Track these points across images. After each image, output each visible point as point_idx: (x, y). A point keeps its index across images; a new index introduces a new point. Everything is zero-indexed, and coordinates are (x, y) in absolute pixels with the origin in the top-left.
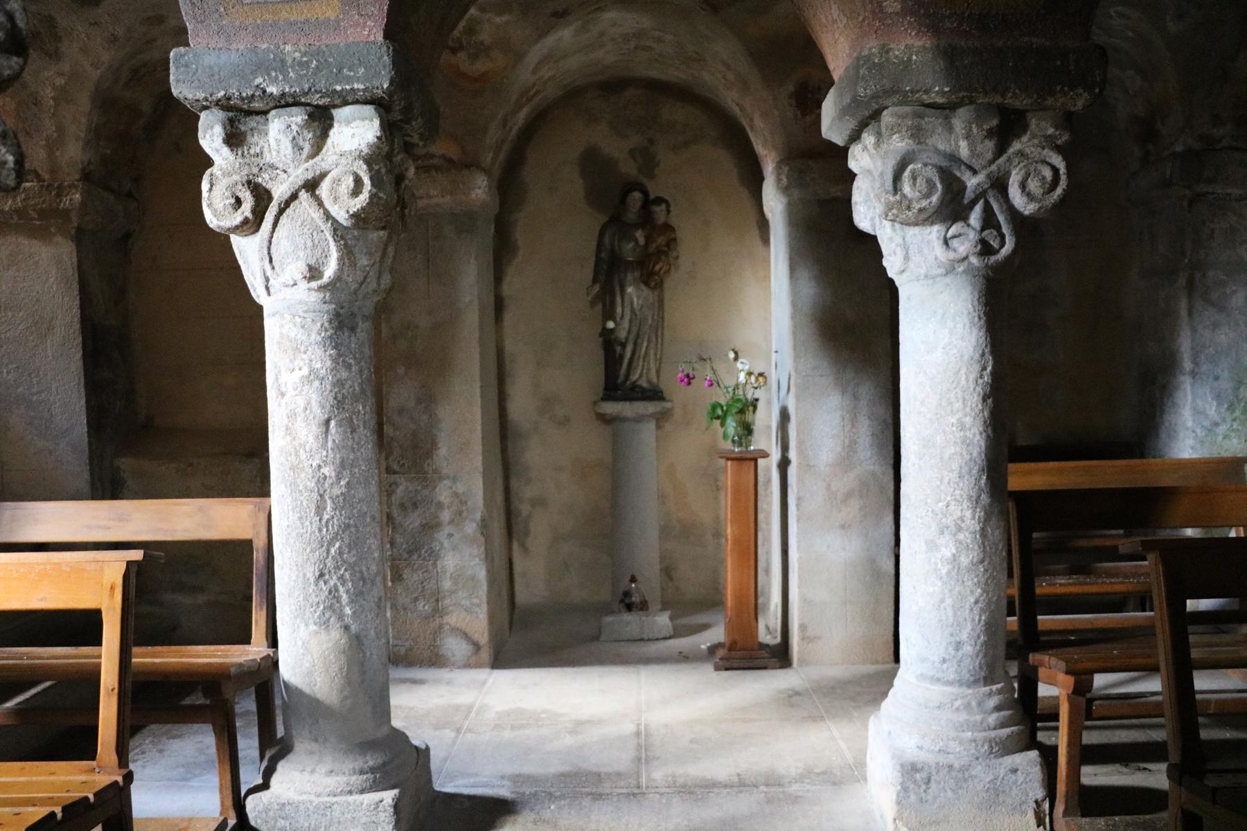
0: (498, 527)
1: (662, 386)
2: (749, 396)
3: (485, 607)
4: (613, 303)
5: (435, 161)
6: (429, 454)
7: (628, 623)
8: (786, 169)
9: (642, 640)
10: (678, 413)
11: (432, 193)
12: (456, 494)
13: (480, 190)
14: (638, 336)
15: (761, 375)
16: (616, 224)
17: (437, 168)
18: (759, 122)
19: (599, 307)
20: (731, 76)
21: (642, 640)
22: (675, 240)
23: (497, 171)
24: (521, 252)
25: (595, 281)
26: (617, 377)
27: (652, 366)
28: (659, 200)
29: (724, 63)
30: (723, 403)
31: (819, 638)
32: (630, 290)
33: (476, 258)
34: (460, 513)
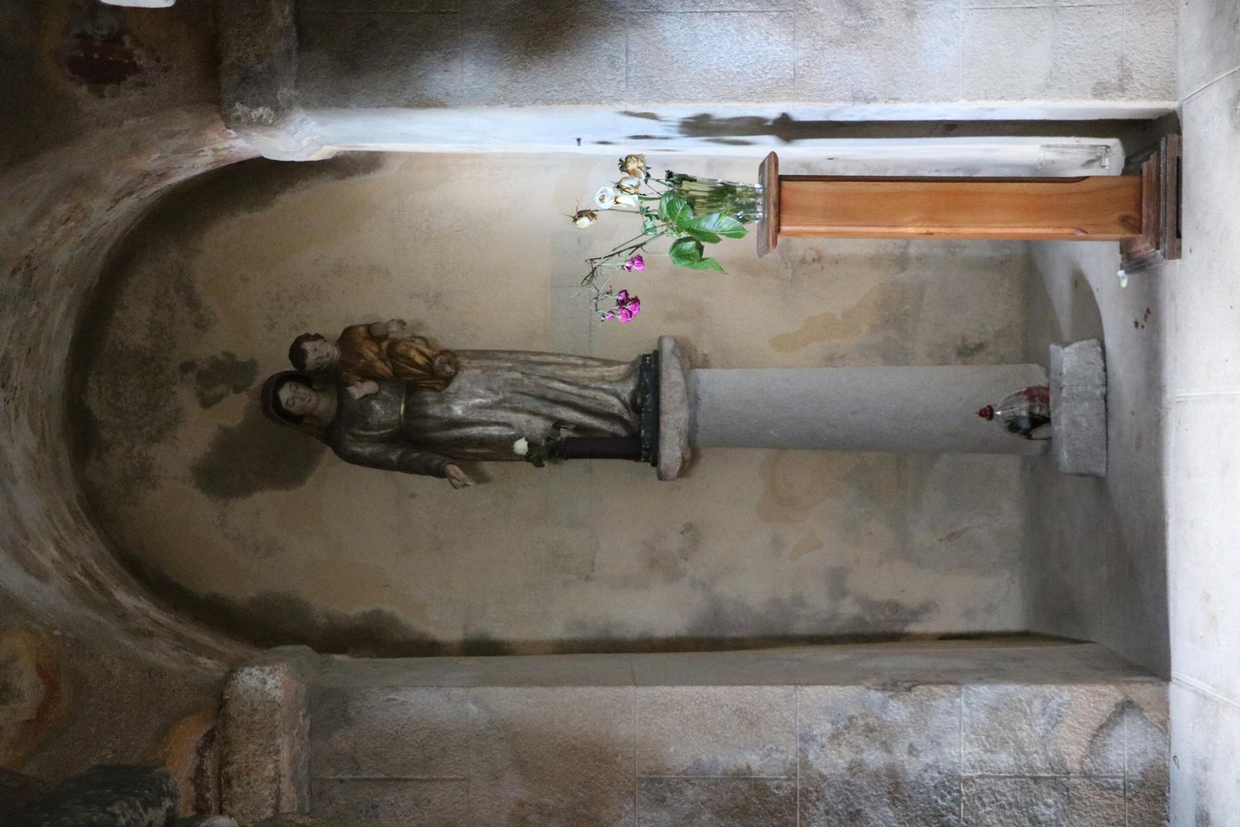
0: (890, 659)
1: (634, 356)
2: (664, 189)
3: (1049, 689)
4: (483, 442)
5: (210, 765)
6: (759, 786)
7: (1074, 422)
8: (240, 109)
9: (1105, 398)
10: (680, 329)
11: (270, 771)
12: (834, 737)
13: (267, 681)
14: (543, 398)
15: (623, 166)
16: (336, 433)
17: (223, 762)
18: (151, 161)
19: (487, 467)
20: (61, 209)
21: (1105, 398)
22: (369, 327)
23: (234, 649)
24: (387, 608)
25: (440, 473)
26: (615, 436)
27: (596, 373)
28: (297, 353)
29: (33, 221)
30: (676, 237)
31: (1122, 59)
32: (458, 411)
33: (395, 688)
34: (870, 730)
